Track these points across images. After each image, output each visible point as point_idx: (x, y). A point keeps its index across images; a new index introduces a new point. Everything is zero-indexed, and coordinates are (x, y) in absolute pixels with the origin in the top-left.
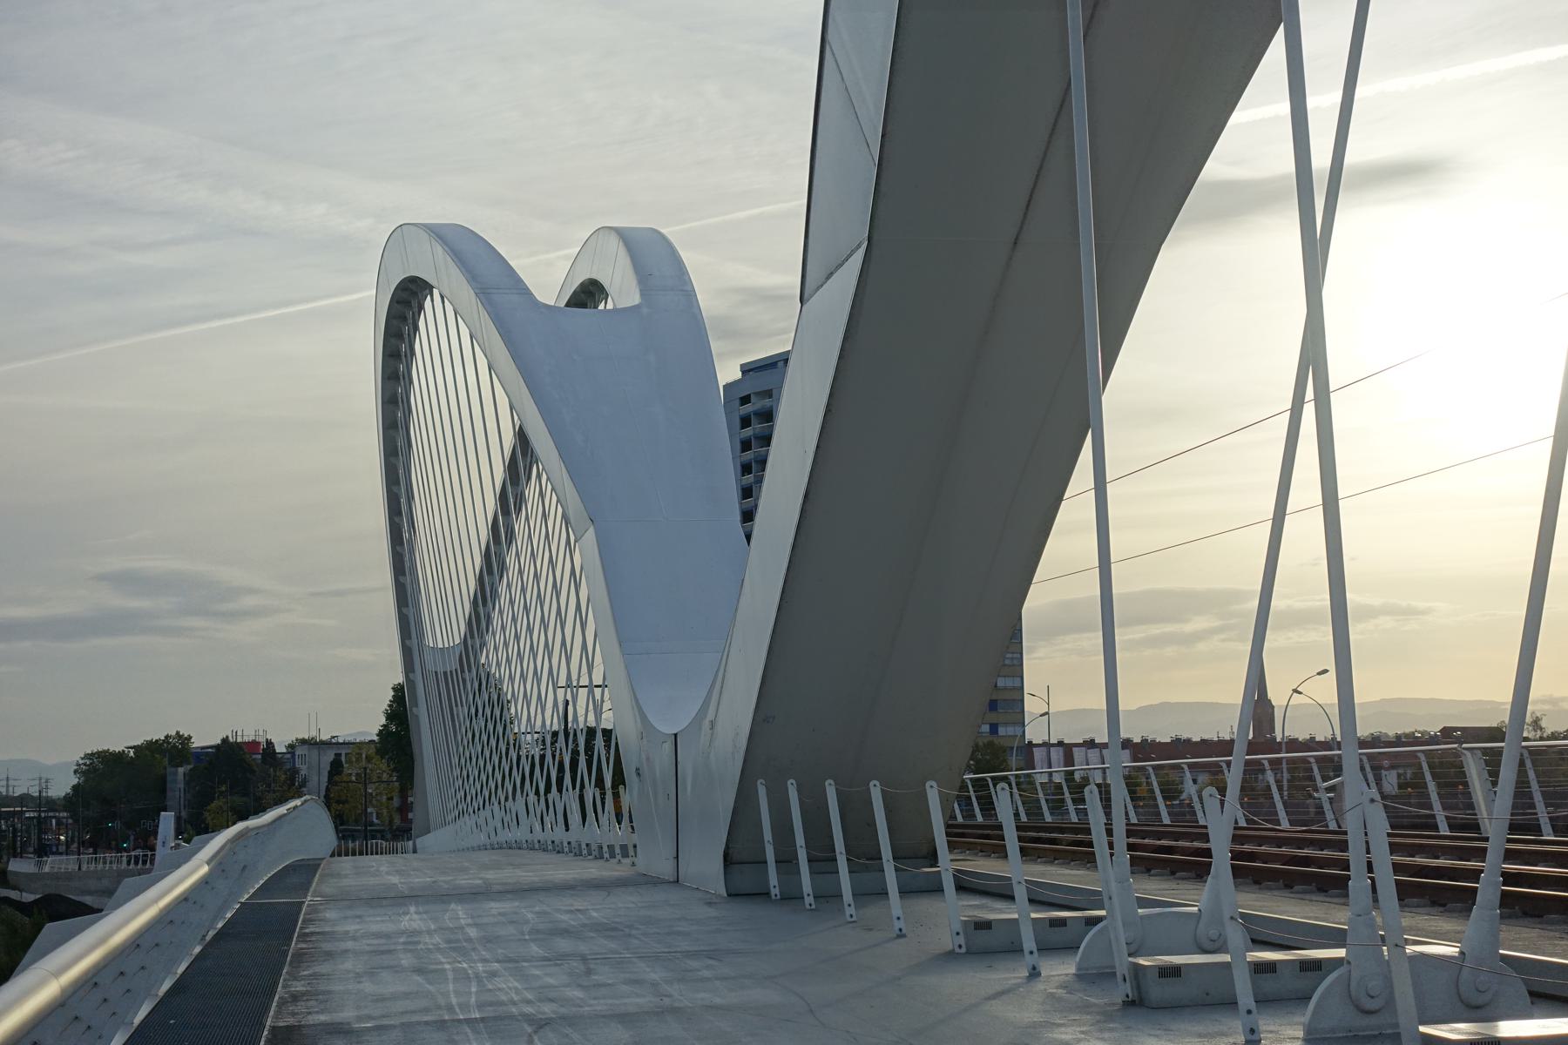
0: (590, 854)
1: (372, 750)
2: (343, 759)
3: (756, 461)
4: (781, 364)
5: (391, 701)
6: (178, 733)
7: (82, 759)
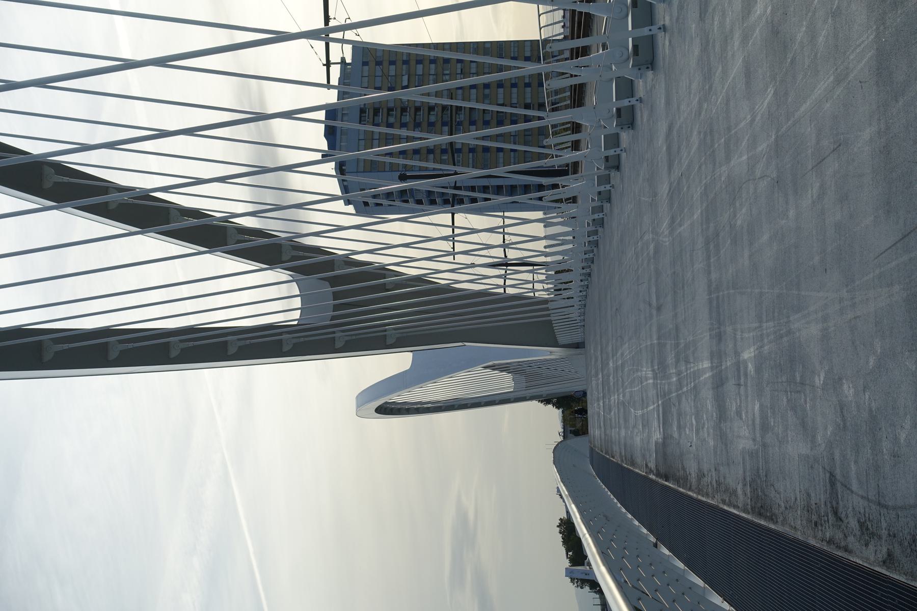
0: (590, 267)
1: (568, 412)
2: (573, 429)
3: (401, 198)
4: (345, 183)
5: (539, 402)
6: (558, 526)
7: (574, 584)
